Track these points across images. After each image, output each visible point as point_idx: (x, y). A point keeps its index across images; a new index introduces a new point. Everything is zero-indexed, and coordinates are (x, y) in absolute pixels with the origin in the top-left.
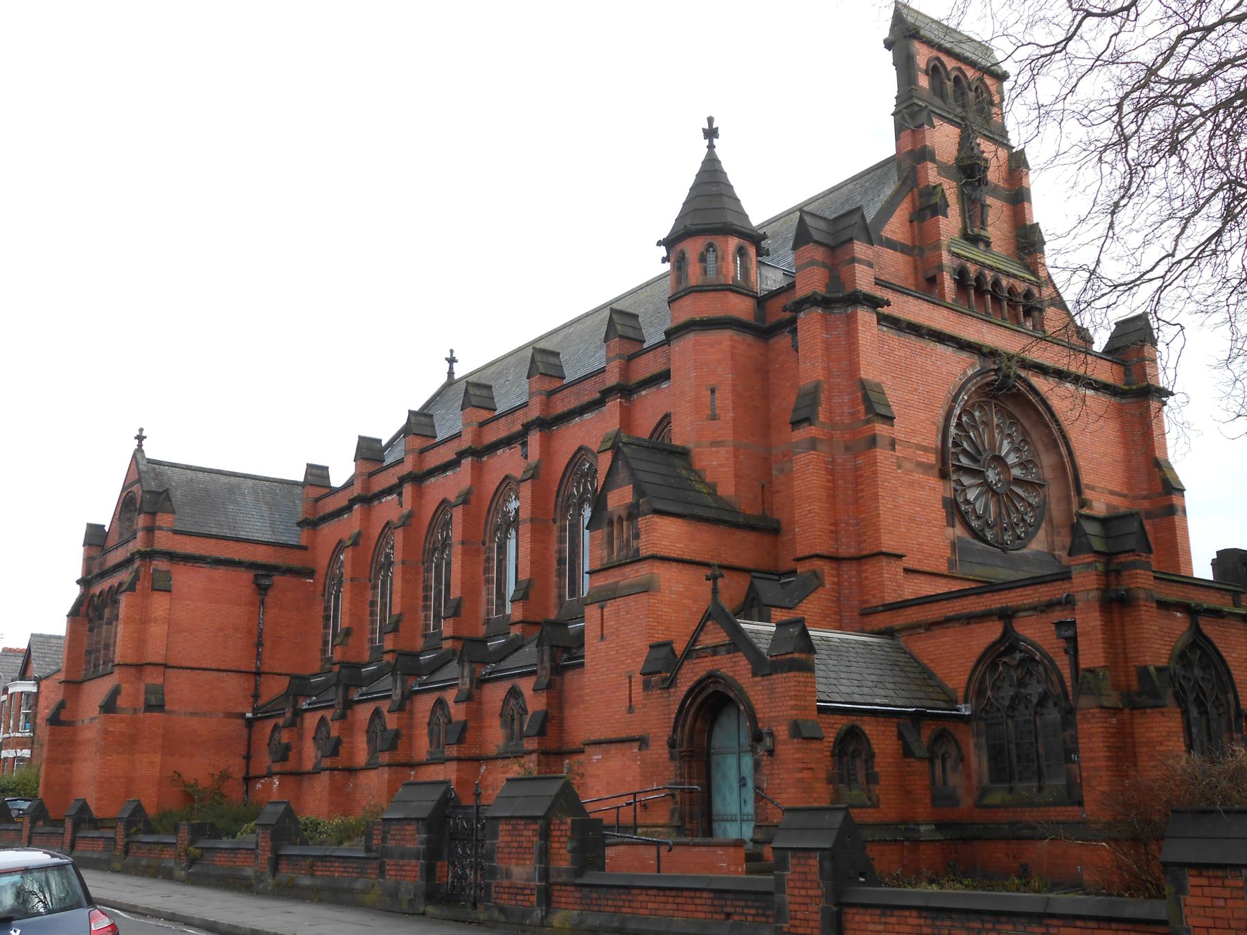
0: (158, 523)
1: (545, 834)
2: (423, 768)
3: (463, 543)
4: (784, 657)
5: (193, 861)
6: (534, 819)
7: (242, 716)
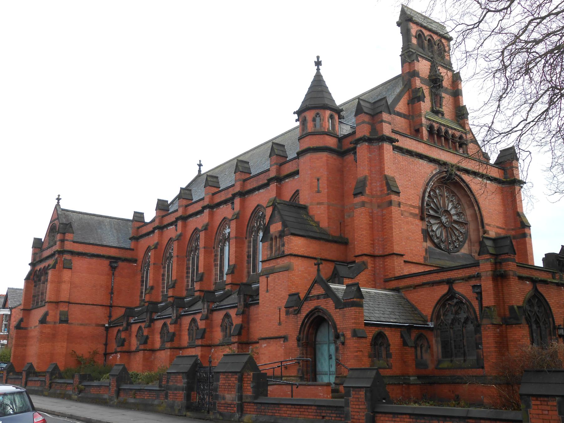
0: (66, 238)
1: (241, 380)
2: (185, 350)
3: (204, 248)
4: (349, 300)
5: (80, 391)
6: (236, 373)
7: (104, 325)
